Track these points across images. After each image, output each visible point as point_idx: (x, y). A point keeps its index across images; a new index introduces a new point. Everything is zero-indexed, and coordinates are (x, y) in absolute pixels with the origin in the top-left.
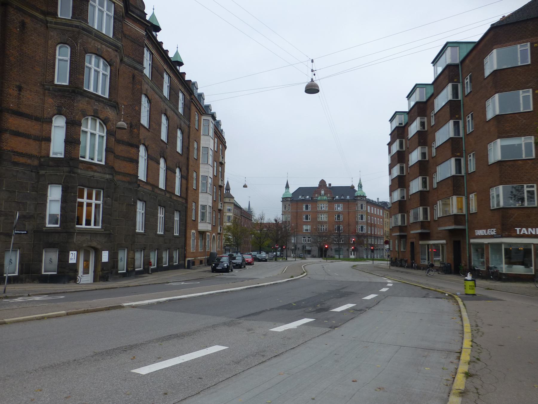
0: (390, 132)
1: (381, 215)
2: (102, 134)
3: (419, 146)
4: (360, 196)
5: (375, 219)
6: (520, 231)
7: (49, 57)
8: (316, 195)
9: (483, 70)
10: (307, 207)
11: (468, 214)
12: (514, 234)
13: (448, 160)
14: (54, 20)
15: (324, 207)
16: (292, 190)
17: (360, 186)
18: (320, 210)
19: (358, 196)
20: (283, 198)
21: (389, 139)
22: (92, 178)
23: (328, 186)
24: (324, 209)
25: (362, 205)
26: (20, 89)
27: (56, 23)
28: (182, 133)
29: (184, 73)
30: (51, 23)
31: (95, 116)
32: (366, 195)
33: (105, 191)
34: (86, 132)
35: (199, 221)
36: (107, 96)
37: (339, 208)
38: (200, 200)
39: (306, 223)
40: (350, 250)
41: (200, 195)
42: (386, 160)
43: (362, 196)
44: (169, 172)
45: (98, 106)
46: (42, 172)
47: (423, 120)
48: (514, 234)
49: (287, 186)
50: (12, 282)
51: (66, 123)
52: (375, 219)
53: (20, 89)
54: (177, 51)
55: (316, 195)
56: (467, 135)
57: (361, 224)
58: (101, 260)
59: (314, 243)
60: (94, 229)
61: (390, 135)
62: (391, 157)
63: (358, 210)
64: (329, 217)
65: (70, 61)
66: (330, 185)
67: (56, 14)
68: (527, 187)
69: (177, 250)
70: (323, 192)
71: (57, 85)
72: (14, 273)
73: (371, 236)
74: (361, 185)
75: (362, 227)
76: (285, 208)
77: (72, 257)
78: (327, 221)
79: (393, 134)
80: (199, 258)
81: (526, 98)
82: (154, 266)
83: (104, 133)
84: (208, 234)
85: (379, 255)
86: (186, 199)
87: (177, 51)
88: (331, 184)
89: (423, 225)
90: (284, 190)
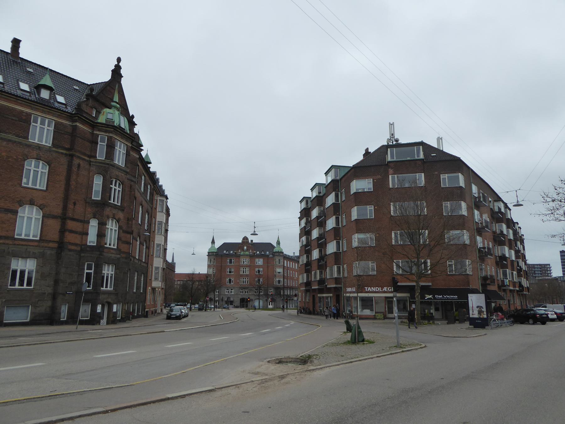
2: (116, 229)
4: (278, 252)
5: (291, 272)
7: (89, 183)
8: (240, 250)
12: (364, 291)
13: (332, 241)
14: (95, 160)
15: (245, 261)
16: (218, 245)
17: (278, 243)
18: (242, 264)
19: (276, 252)
20: (209, 253)
21: (299, 215)
22: (110, 258)
23: (250, 242)
25: (279, 260)
26: (75, 204)
27: (96, 162)
28: (148, 215)
29: (150, 167)
30: (93, 162)
31: (114, 218)
32: (283, 251)
33: (116, 265)
34: (108, 228)
35: (153, 280)
37: (260, 262)
40: (268, 301)
41: (155, 259)
42: (297, 231)
44: (141, 245)
45: (115, 211)
46: (82, 255)
48: (364, 291)
49: (213, 242)
50: (64, 324)
51: (98, 224)
52: (291, 272)
54: (147, 153)
56: (343, 227)
58: (113, 311)
60: (106, 290)
63: (276, 265)
66: (252, 241)
67: (96, 157)
69: (120, 303)
70: (245, 248)
71: (94, 200)
73: (287, 288)
74: (279, 242)
76: (211, 261)
77: (99, 309)
78: (248, 275)
80: (151, 309)
81: (371, 210)
82: (119, 317)
83: (116, 228)
84: (157, 289)
85: (294, 305)
86: (148, 264)
87: (147, 153)
88: (252, 240)
90: (209, 245)
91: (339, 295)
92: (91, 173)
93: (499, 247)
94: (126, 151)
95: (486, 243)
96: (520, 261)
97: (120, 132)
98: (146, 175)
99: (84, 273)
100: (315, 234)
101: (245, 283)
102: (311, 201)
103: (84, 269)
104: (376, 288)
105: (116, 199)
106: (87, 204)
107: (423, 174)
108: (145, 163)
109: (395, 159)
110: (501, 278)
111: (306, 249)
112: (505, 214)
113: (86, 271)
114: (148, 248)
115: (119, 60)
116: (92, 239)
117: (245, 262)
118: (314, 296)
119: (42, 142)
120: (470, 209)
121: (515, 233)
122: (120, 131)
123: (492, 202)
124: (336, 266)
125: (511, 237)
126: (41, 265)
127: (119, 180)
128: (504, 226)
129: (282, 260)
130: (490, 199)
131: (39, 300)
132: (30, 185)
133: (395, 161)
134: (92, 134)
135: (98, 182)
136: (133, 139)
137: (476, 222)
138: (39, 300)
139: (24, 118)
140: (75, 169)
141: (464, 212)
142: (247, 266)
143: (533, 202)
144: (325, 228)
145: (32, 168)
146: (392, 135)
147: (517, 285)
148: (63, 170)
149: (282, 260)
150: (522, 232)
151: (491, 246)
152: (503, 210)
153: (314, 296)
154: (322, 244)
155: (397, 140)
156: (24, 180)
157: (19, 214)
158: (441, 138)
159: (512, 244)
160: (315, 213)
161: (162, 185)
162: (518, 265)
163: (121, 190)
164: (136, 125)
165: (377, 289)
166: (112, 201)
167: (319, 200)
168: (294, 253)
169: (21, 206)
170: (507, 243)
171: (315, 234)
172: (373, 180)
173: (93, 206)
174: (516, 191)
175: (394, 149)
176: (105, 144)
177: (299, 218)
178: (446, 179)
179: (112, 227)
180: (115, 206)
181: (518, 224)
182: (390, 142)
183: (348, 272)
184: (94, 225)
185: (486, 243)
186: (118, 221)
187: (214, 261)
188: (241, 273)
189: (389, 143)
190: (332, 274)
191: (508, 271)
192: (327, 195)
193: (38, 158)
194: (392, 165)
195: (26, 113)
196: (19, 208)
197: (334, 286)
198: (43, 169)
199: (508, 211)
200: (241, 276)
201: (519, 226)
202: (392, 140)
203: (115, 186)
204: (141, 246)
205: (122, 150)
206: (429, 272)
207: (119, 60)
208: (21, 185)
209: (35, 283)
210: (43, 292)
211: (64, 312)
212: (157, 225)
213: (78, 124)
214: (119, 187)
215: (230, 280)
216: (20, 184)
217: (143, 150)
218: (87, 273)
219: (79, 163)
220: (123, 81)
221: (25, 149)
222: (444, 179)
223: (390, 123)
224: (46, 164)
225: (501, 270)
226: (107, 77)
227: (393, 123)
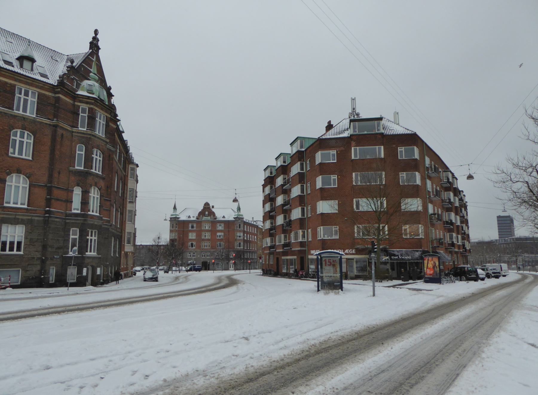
0: (264, 179)
1: (256, 232)
3: (282, 194)
8: (201, 215)
9: (315, 162)
11: (307, 241)
21: (263, 183)
24: (207, 228)
26: (59, 173)
27: (78, 133)
30: (75, 132)
31: (96, 185)
38: (127, 228)
42: (261, 198)
51: (82, 191)
53: (59, 173)
56: (308, 194)
57: (239, 241)
61: (264, 180)
62: (265, 196)
64: (211, 235)
65: (85, 154)
70: (207, 213)
72: (18, 283)
75: (240, 244)
81: (334, 180)
83: (98, 195)
84: (128, 254)
89: (285, 245)
91: (303, 257)
92: (73, 144)
93: (447, 213)
94: (105, 122)
95: (436, 210)
96: (464, 225)
97: (100, 104)
98: (120, 145)
99: (69, 238)
100: (280, 200)
101: (207, 247)
103: (69, 235)
105: (97, 169)
106: (71, 173)
107: (382, 147)
108: (120, 133)
109: (357, 133)
110: (447, 241)
111: (269, 216)
113: (71, 237)
114: (122, 214)
115: (96, 32)
116: (76, 207)
117: (207, 227)
118: (278, 259)
119: (26, 112)
120: (423, 179)
121: (461, 200)
123: (442, 172)
124: (300, 231)
125: (457, 204)
126: (30, 231)
128: (452, 194)
129: (242, 225)
130: (440, 170)
131: (28, 265)
132: (16, 155)
133: (357, 135)
134: (74, 105)
135: (80, 151)
137: (428, 191)
138: (28, 265)
139: (8, 89)
140: (59, 139)
141: (418, 182)
142: (208, 231)
143: (469, 170)
144: (289, 196)
145: (18, 139)
146: (354, 109)
147: (462, 247)
148: (47, 140)
149: (242, 225)
150: (466, 199)
151: (440, 213)
152: (451, 180)
153: (278, 259)
154: (286, 210)
155: (358, 115)
156: (11, 150)
157: (7, 183)
158: (397, 113)
159: (457, 211)
160: (279, 181)
162: (462, 230)
163: (101, 159)
164: (113, 96)
166: (93, 171)
167: (284, 170)
168: (253, 218)
169: (9, 175)
170: (454, 210)
171: (280, 200)
174: (469, 165)
175: (357, 122)
176: (86, 115)
178: (402, 152)
180: (97, 175)
181: (463, 192)
182: (352, 116)
183: (312, 237)
184: (77, 193)
185: (436, 210)
188: (203, 237)
189: (351, 117)
190: (296, 237)
191: (454, 235)
192: (292, 164)
193: (24, 128)
194: (354, 138)
195: (11, 84)
196: (7, 177)
197: (299, 249)
198: (28, 140)
199: (455, 180)
200: (203, 241)
201: (464, 194)
202: (354, 114)
203: (96, 155)
204: (117, 212)
205: (102, 121)
207: (96, 32)
208: (8, 155)
209: (25, 248)
210: (33, 257)
211: (52, 272)
212: (128, 192)
213: (61, 96)
214: (100, 157)
215: (192, 245)
216: (7, 154)
218: (72, 238)
219: (62, 133)
220: (102, 54)
221: (10, 120)
222: (401, 152)
223: (352, 98)
224: (31, 134)
225: (448, 234)
226: (86, 49)
227: (355, 98)
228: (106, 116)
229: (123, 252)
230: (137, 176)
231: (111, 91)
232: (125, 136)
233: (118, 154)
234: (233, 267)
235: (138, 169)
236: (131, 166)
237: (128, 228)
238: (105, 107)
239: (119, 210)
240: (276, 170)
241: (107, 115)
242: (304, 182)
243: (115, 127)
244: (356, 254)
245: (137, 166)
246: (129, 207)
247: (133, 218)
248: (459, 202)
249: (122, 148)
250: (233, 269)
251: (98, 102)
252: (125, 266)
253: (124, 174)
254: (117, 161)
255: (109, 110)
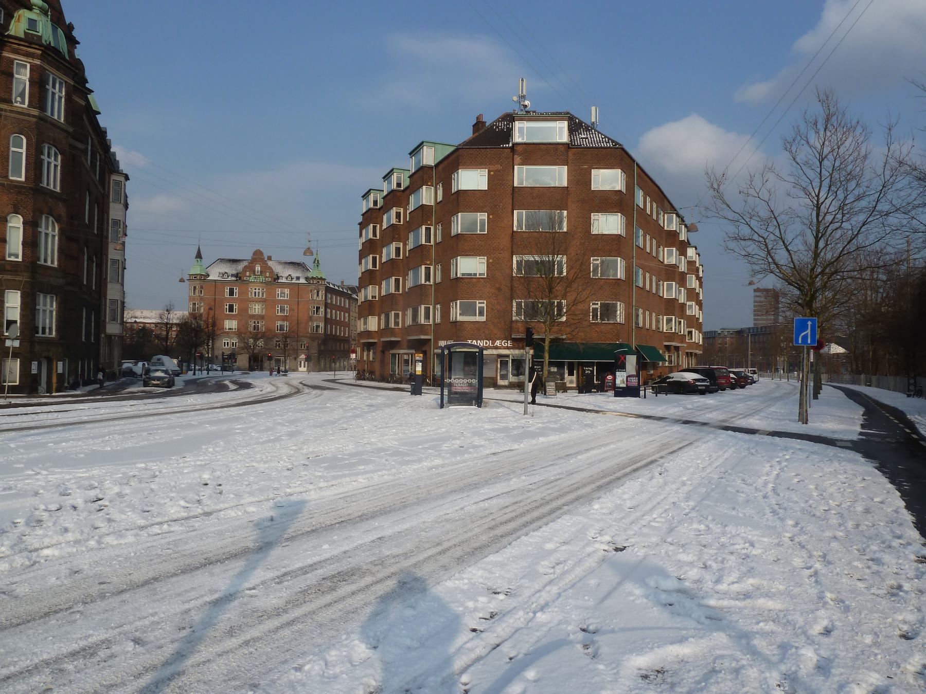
6: (471, 342)
8: (248, 273)
10: (231, 292)
14: (10, 108)
21: (360, 219)
27: (11, 111)
35: (107, 320)
36: (58, 189)
39: (230, 318)
43: (318, 279)
47: (398, 211)
55: (248, 273)
57: (316, 320)
59: (243, 349)
68: (479, 303)
70: (258, 268)
79: (366, 215)
81: (482, 221)
84: (113, 338)
97: (53, 57)
102: (382, 197)
104: (673, 331)
105: (53, 180)
108: (92, 114)
112: (679, 234)
122: (54, 56)
127: (55, 147)
133: (525, 144)
136: (76, 71)
137: (638, 247)
161: (115, 152)
163: (59, 162)
164: (78, 43)
165: (486, 343)
170: (677, 277)
172: (489, 171)
173: (12, 191)
177: (360, 224)
179: (54, 231)
186: (58, 219)
187: (201, 291)
194: (519, 148)
203: (49, 156)
206: (564, 319)
214: (56, 159)
217: (93, 92)
228: (66, 82)
229: (103, 335)
230: (126, 196)
231: (74, 33)
232: (102, 121)
233: (89, 153)
234: (304, 367)
235: (128, 183)
236: (115, 177)
237: (112, 292)
238: (63, 65)
239: (95, 260)
240: (384, 198)
241: (66, 80)
242: (431, 222)
243: (83, 103)
244: (513, 348)
245: (127, 178)
246: (113, 254)
247: (120, 274)
248: (49, 390)
249: (96, 142)
250: (305, 369)
251: (50, 53)
252: (661, 317)
253: (102, 192)
254: (88, 168)
255: (72, 70)
